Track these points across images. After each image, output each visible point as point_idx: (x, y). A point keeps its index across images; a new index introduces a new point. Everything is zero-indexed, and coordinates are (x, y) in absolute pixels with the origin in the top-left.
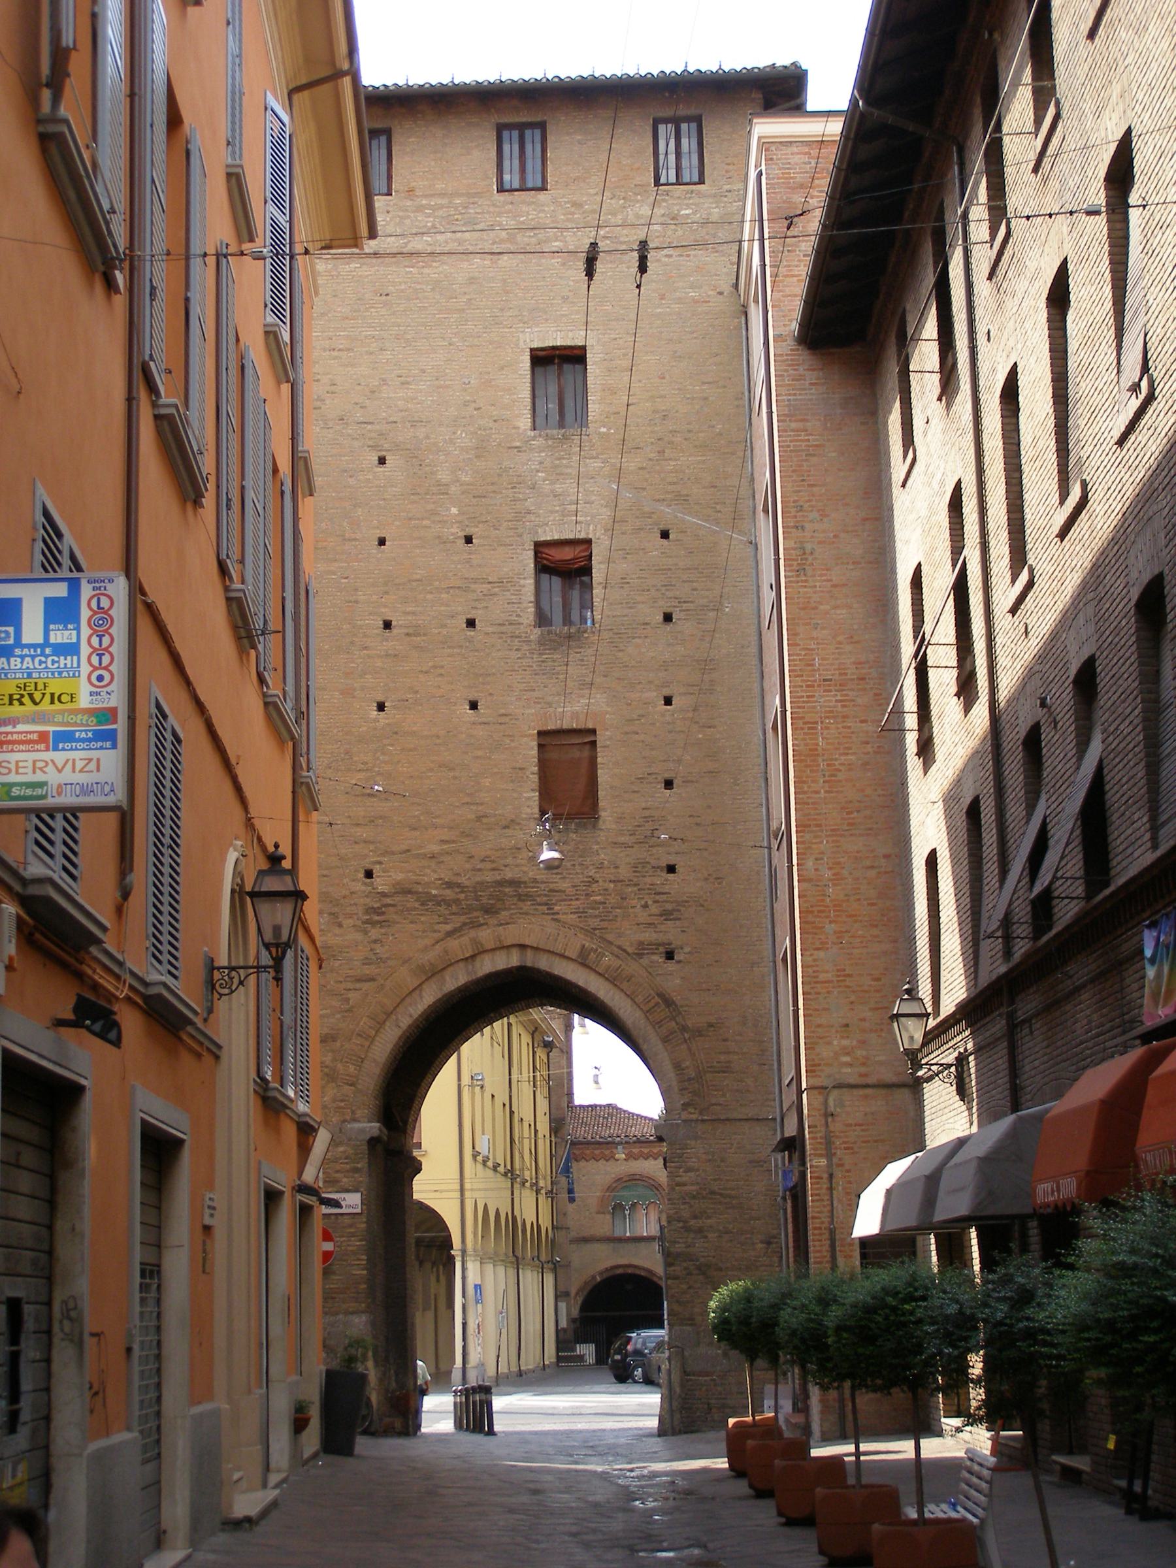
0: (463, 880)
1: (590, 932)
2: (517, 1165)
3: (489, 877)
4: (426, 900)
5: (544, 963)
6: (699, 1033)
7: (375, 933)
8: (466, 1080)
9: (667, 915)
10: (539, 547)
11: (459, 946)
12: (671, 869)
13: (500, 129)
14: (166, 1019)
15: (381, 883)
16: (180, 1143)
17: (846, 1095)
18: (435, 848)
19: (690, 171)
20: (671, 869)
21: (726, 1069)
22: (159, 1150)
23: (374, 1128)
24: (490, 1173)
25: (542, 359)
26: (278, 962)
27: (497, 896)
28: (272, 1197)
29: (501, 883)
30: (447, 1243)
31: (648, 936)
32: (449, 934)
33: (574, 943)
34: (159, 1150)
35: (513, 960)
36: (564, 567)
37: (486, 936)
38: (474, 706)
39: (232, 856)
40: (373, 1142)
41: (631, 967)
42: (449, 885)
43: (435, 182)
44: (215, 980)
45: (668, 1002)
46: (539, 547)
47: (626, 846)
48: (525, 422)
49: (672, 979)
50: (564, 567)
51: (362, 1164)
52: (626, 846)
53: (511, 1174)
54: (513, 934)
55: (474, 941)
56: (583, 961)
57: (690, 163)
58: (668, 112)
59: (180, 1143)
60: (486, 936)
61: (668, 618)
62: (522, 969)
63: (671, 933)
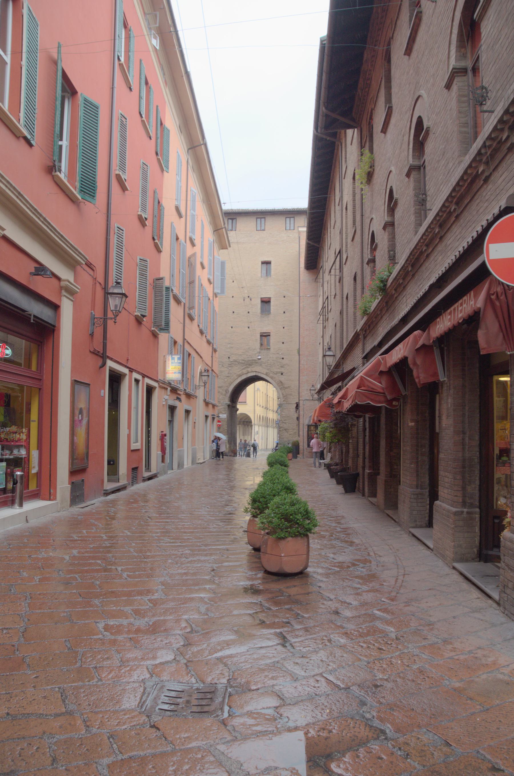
0: (246, 359)
1: (268, 369)
2: (268, 406)
3: (250, 359)
4: (239, 363)
5: (259, 375)
6: (286, 388)
7: (230, 368)
8: (256, 389)
9: (282, 367)
10: (261, 298)
11: (245, 371)
12: (283, 358)
13: (257, 218)
14: (189, 396)
15: (231, 360)
16: (190, 411)
17: (307, 401)
18: (241, 353)
19: (292, 228)
20: (283, 358)
21: (291, 395)
22: (187, 412)
23: (229, 403)
24: (261, 408)
25: (263, 263)
26: (205, 385)
27: (250, 363)
28: (207, 417)
29: (253, 360)
30: (251, 422)
31: (279, 370)
32: (243, 369)
33: (265, 371)
34: (187, 412)
35: (254, 374)
36: (266, 302)
37: (249, 370)
38: (249, 328)
39: (200, 367)
40: (229, 406)
41: (275, 376)
42: (243, 360)
43: (242, 233)
44: (196, 387)
45: (281, 382)
46: (261, 298)
47: (275, 354)
48: (260, 275)
49: (282, 378)
50: (266, 302)
51: (227, 409)
52: (275, 354)
53: (267, 408)
54: (254, 369)
55: (248, 371)
56: (266, 374)
57: (292, 225)
58: (289, 216)
59: (190, 411)
60: (249, 370)
61: (284, 312)
62: (256, 376)
63: (282, 370)
